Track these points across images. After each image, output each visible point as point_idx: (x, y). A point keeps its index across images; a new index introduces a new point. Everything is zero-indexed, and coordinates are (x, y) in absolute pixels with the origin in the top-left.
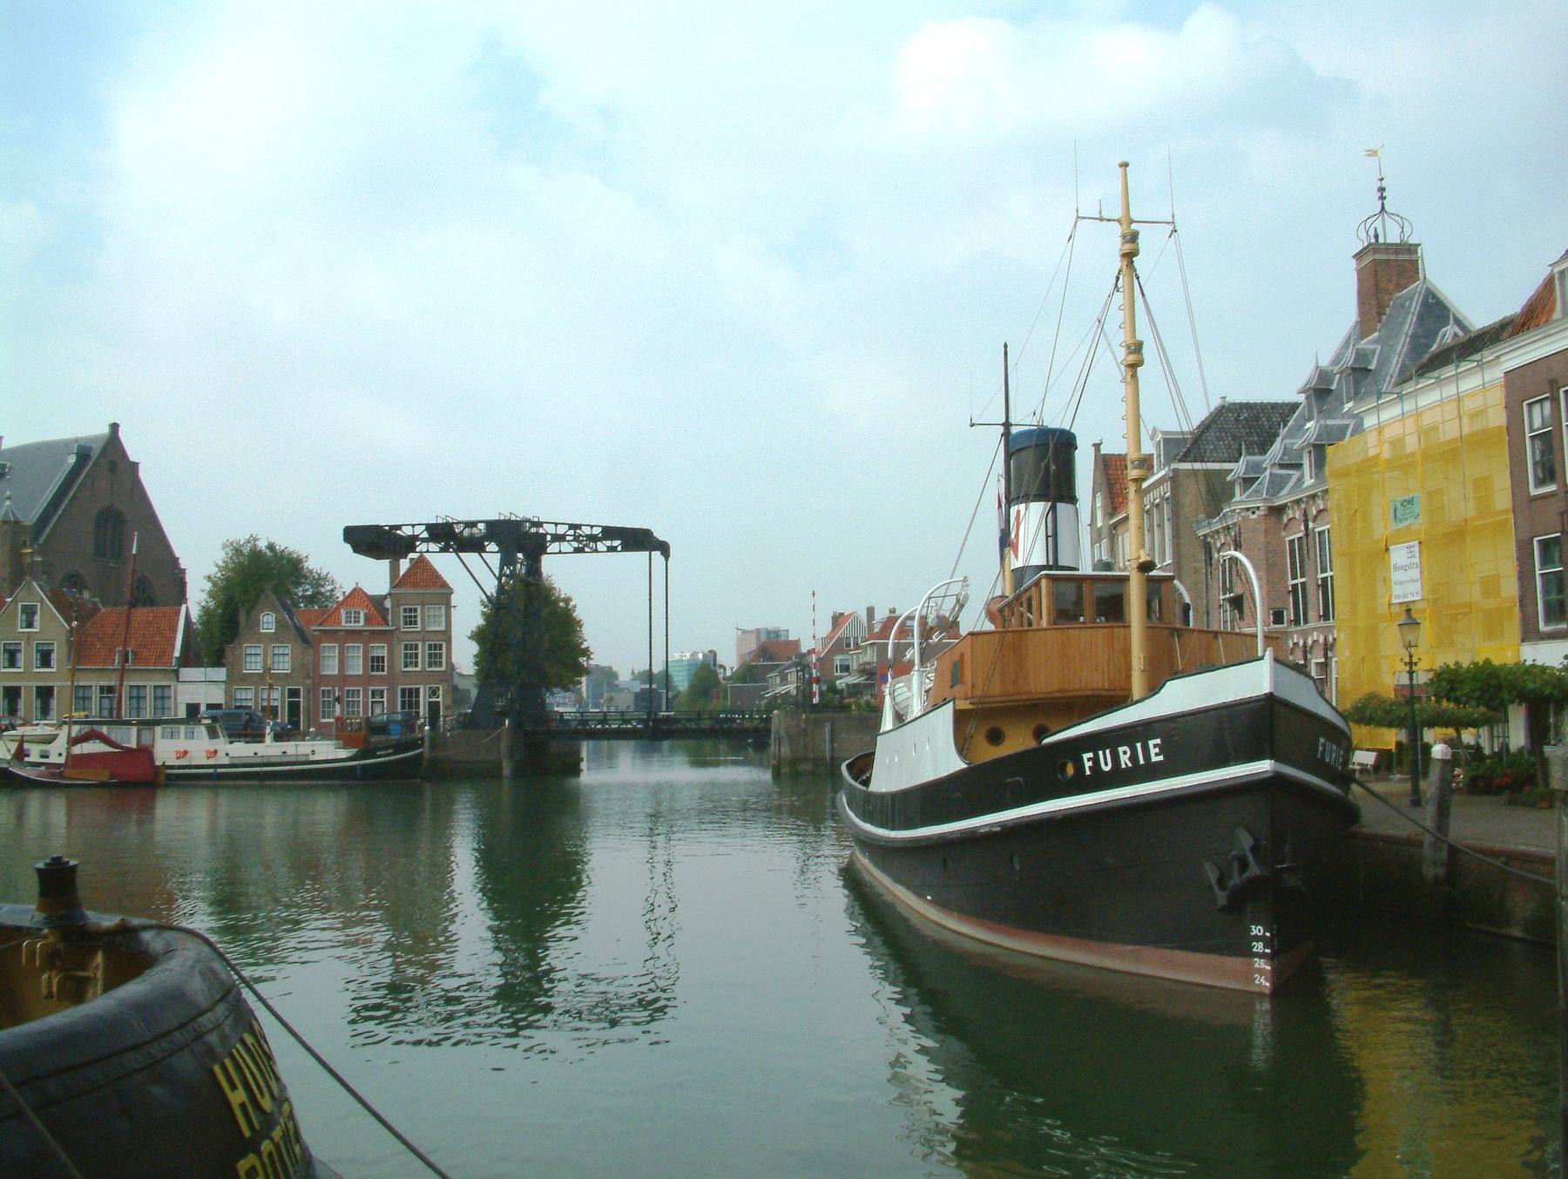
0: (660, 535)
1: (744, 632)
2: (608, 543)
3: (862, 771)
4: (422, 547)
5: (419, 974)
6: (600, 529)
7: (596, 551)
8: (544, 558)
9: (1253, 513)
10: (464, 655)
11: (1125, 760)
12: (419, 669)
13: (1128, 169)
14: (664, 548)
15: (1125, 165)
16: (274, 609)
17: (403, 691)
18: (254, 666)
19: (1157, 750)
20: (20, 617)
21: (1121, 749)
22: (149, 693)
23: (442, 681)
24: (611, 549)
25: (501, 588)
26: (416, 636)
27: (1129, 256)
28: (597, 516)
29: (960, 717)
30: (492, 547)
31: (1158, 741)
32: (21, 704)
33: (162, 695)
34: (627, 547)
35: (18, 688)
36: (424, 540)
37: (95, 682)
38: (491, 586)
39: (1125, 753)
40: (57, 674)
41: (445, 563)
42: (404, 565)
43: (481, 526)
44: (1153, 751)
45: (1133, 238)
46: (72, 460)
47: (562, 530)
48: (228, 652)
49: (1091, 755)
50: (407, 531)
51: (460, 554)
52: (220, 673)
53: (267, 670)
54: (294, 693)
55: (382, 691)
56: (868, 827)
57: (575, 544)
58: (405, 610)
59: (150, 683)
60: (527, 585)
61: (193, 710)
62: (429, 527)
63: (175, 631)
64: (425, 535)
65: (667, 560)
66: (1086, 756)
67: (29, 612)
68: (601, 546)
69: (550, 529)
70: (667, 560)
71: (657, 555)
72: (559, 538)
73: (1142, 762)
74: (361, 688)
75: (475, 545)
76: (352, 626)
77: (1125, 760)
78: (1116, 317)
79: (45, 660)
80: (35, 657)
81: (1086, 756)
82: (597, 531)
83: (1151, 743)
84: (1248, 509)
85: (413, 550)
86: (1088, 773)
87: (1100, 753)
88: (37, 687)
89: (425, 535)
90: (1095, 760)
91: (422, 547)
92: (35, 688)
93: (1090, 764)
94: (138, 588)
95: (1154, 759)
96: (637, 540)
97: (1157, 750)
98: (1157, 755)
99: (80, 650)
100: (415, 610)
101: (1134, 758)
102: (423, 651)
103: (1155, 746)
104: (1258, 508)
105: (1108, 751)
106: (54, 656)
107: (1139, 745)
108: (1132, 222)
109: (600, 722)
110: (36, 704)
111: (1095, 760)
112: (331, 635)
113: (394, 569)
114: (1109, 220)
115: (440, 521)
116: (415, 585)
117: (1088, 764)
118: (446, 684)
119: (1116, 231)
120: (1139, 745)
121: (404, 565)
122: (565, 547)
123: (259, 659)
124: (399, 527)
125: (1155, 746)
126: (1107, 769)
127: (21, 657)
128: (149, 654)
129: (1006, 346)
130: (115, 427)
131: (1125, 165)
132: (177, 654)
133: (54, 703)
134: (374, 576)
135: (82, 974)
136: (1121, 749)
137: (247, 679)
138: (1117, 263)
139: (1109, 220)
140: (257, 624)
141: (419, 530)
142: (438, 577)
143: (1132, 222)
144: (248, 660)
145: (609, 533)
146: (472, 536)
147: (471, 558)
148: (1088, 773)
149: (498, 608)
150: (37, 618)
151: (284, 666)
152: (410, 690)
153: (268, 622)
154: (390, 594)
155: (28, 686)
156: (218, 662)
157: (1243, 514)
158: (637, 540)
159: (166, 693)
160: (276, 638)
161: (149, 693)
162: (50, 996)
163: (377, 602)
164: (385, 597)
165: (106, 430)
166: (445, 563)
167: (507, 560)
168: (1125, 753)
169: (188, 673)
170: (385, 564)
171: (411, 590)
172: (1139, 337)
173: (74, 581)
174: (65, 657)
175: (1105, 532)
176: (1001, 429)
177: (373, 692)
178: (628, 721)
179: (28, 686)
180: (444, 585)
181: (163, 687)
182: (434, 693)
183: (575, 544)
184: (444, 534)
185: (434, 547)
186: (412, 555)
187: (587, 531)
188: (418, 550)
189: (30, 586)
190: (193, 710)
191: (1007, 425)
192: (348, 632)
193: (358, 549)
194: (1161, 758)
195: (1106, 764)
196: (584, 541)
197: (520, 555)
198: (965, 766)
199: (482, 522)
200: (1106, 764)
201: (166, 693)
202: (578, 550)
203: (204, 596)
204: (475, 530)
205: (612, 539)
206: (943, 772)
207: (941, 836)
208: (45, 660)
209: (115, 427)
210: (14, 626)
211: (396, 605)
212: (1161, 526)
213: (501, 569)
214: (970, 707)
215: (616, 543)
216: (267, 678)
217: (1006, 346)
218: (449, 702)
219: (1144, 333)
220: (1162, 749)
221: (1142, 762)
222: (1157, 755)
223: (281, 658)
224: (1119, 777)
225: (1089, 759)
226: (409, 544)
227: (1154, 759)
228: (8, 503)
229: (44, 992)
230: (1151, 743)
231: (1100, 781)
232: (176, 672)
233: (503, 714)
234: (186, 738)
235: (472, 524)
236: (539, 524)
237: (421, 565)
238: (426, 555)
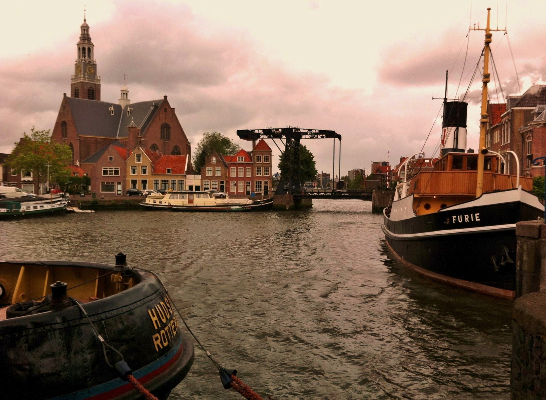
0: (338, 132)
1: (374, 163)
2: (321, 135)
3: (388, 214)
4: (262, 137)
5: (538, 106)
6: (318, 131)
7: (317, 138)
8: (301, 140)
9: (538, 126)
10: (275, 170)
11: (467, 219)
12: (269, 175)
13: (490, 11)
14: (339, 137)
15: (489, 9)
16: (216, 156)
17: (256, 182)
18: (209, 174)
19: (478, 217)
20: (136, 158)
21: (466, 216)
22: (177, 182)
23: (268, 179)
24: (322, 137)
25: (287, 149)
26: (260, 165)
27: (487, 43)
28: (317, 127)
29: (415, 199)
30: (284, 137)
31: (478, 214)
32: (137, 185)
33: (181, 183)
34: (327, 137)
35: (136, 181)
36: (262, 134)
37: (160, 179)
38: (283, 149)
39: (467, 217)
40: (148, 176)
41: (269, 141)
42: (257, 142)
43: (280, 130)
44: (477, 217)
45: (489, 36)
46: (152, 108)
47: (306, 131)
48: (202, 169)
49: (455, 217)
50: (257, 132)
51: (274, 139)
52: (199, 177)
53: (214, 175)
54: (222, 183)
55: (250, 182)
56: (388, 231)
57: (311, 136)
58: (257, 157)
59: (177, 179)
60: (295, 149)
61: (191, 188)
62: (264, 130)
63: (185, 163)
64: (262, 133)
65: (340, 141)
66: (454, 217)
67: (139, 157)
68: (319, 136)
69: (302, 131)
70: (340, 141)
71: (337, 140)
72: (306, 134)
73: (472, 220)
74: (251, 181)
75: (279, 136)
76: (241, 161)
77: (467, 219)
78: (482, 65)
79: (144, 172)
80: (141, 171)
81: (454, 217)
82: (317, 131)
83: (476, 214)
84: (536, 124)
85: (259, 138)
86: (454, 222)
87: (459, 216)
88: (132, 180)
89: (262, 133)
90: (457, 219)
91: (262, 137)
92: (141, 181)
93: (455, 220)
94: (175, 149)
95: (477, 220)
96: (331, 134)
97: (478, 217)
98: (478, 218)
99: (155, 170)
100: (260, 157)
101: (470, 219)
102: (263, 169)
103: (477, 216)
104: (540, 124)
105: (461, 216)
106: (147, 171)
107: (472, 215)
108: (490, 30)
109: (311, 193)
110: (141, 185)
111: (457, 219)
112: (234, 164)
113: (254, 143)
114: (481, 30)
115: (267, 128)
116: (260, 149)
117: (454, 220)
118: (270, 180)
119: (484, 33)
120: (472, 215)
121: (257, 142)
122: (308, 137)
123: (211, 172)
124: (254, 130)
125: (477, 216)
126: (460, 222)
127: (136, 171)
128: (178, 170)
129: (447, 71)
130: (166, 97)
131: (489, 9)
132: (186, 170)
133: (147, 185)
134: (247, 146)
135: (126, 284)
136: (466, 216)
137: (207, 178)
138: (483, 45)
139: (481, 30)
140: (211, 161)
141: (260, 131)
142: (268, 146)
143: (490, 30)
144: (208, 172)
145: (321, 132)
146: (277, 133)
147: (277, 140)
148: (454, 222)
149: (285, 157)
150: (141, 158)
151: (219, 174)
152: (259, 182)
153: (214, 160)
154: (252, 152)
155: (139, 180)
156: (199, 173)
157: (534, 126)
158: (331, 134)
159: (182, 182)
160: (217, 165)
161: (177, 182)
162: (118, 289)
163: (249, 153)
164: (251, 152)
165: (163, 98)
166: (269, 141)
167: (288, 141)
168: (467, 217)
169: (188, 176)
170: (251, 142)
171: (258, 150)
172: (489, 72)
173: (154, 147)
174: (150, 171)
175: (489, 131)
176: (443, 100)
177: (247, 182)
178: (327, 193)
179: (139, 180)
180: (270, 149)
181: (181, 180)
182: (266, 183)
183: (311, 136)
184: (269, 133)
185: (266, 137)
186: (259, 139)
187: (314, 131)
188: (261, 137)
189: (139, 148)
190: (191, 188)
191: (445, 99)
192: (239, 163)
193: (241, 137)
194: (479, 220)
195: (460, 220)
196: (313, 135)
197: (293, 139)
198: (415, 216)
199: (280, 129)
200: (460, 220)
201: (182, 182)
202: (311, 138)
203: (196, 150)
204: (278, 131)
205: (322, 134)
206: (409, 217)
207: (408, 238)
208: (144, 172)
209: (166, 97)
210: (134, 160)
211: (254, 155)
212: (507, 130)
213: (286, 143)
214: (418, 197)
215: (324, 135)
216: (213, 178)
217: (447, 71)
218: (271, 186)
219: (490, 71)
220: (480, 217)
221: (472, 220)
222: (478, 218)
223: (209, 172)
224: (465, 225)
225: (455, 218)
226: (258, 135)
227: (477, 220)
228: (132, 121)
229: (117, 288)
230: (476, 214)
231: (458, 225)
232: (186, 176)
233: (286, 190)
234: (180, 199)
235: (277, 129)
236: (299, 129)
237: (262, 142)
238: (264, 139)
